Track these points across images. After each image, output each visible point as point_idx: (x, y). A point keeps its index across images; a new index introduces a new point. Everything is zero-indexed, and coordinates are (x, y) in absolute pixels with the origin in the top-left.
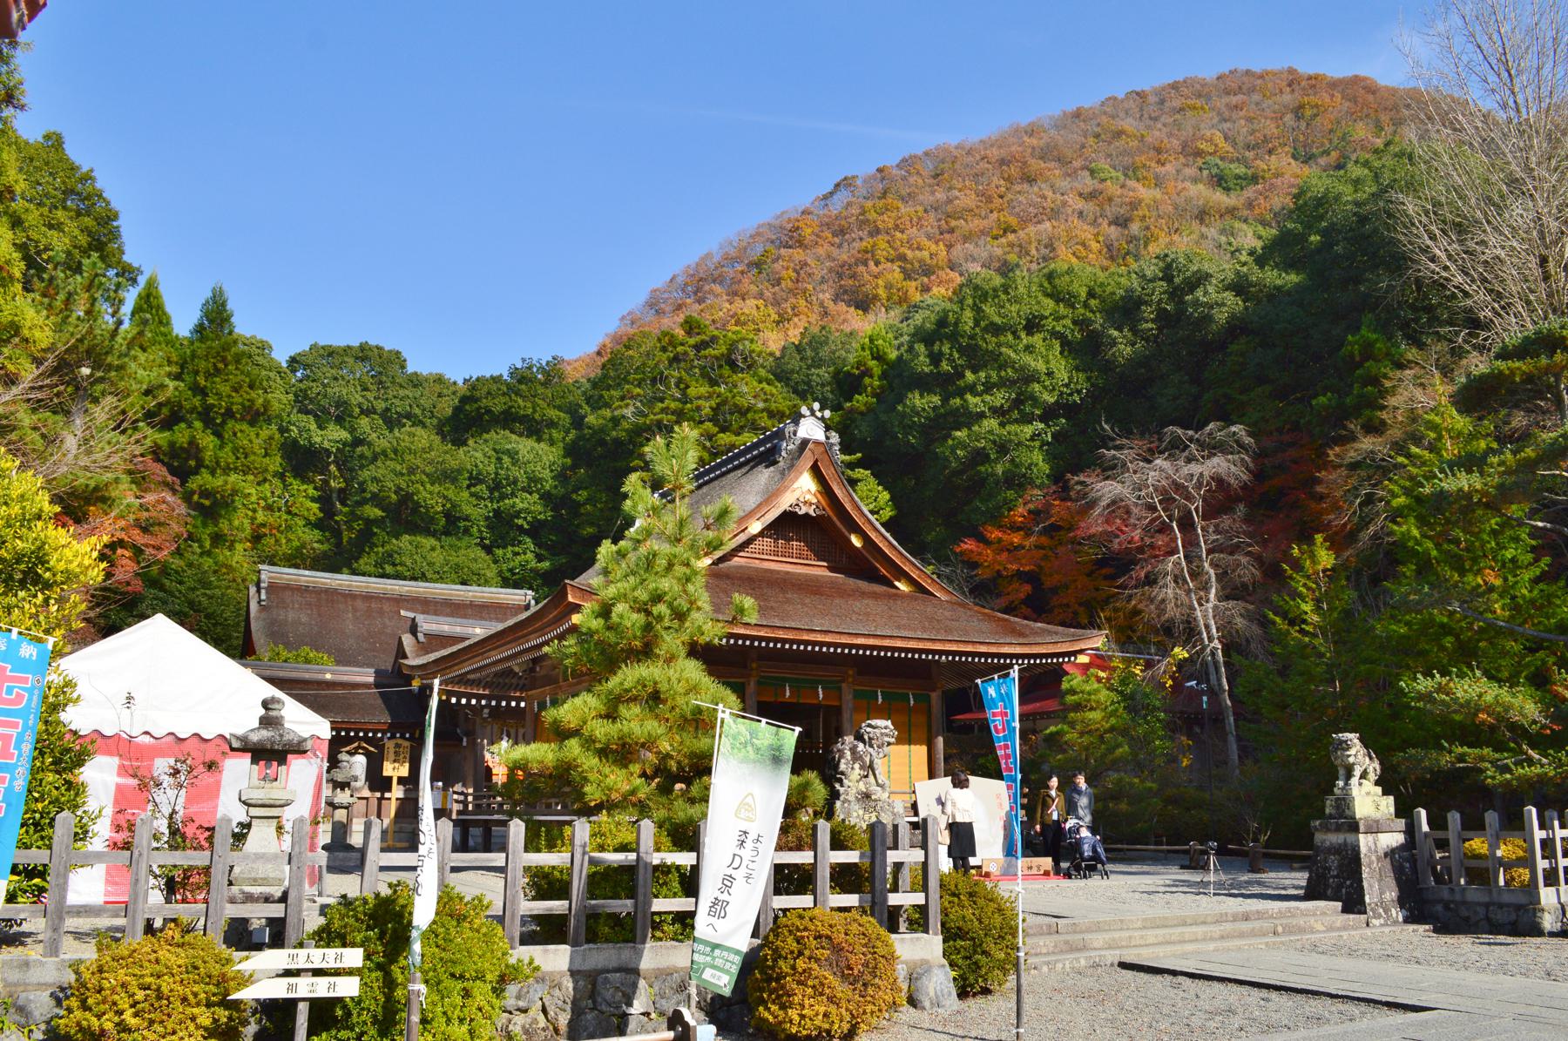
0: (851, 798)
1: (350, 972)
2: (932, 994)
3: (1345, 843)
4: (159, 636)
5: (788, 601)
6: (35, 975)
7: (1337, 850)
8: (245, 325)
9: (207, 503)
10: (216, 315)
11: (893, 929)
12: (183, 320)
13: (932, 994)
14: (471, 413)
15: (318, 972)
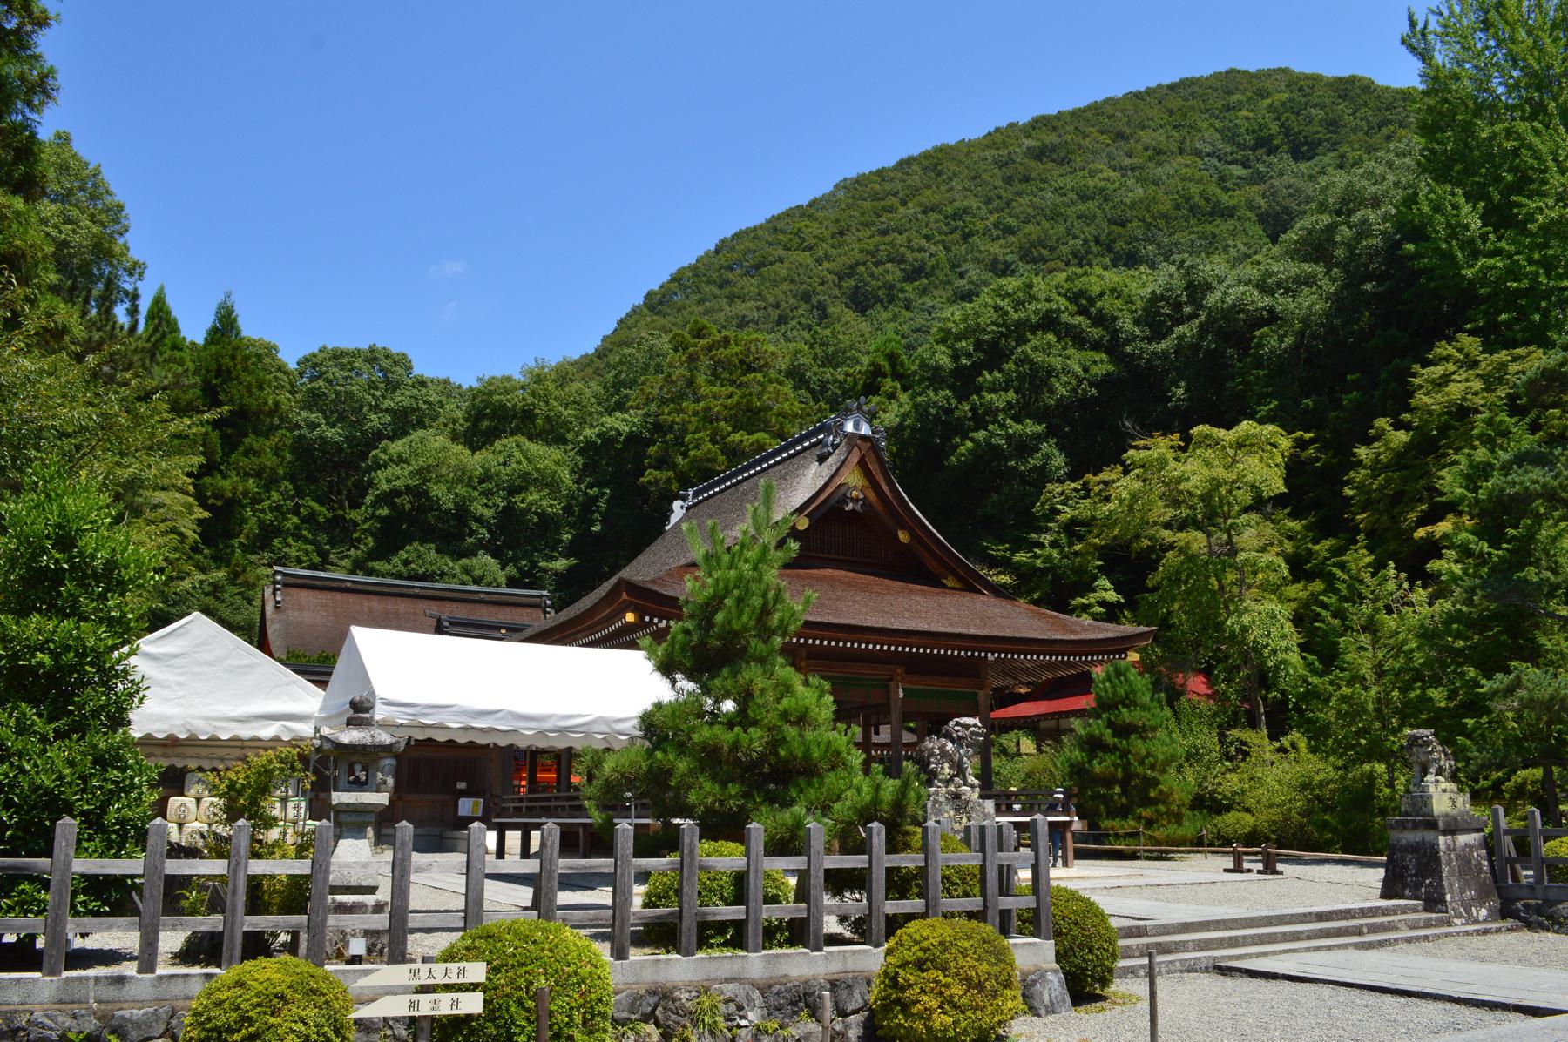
0: (942, 799)
1: (473, 987)
2: (1047, 1001)
3: (1423, 841)
4: (1201, 678)
5: (838, 598)
6: (130, 991)
7: (1415, 848)
8: (251, 328)
9: (219, 503)
10: (225, 324)
11: (1005, 931)
12: (194, 328)
13: (1047, 1001)
14: (490, 416)
15: (448, 988)
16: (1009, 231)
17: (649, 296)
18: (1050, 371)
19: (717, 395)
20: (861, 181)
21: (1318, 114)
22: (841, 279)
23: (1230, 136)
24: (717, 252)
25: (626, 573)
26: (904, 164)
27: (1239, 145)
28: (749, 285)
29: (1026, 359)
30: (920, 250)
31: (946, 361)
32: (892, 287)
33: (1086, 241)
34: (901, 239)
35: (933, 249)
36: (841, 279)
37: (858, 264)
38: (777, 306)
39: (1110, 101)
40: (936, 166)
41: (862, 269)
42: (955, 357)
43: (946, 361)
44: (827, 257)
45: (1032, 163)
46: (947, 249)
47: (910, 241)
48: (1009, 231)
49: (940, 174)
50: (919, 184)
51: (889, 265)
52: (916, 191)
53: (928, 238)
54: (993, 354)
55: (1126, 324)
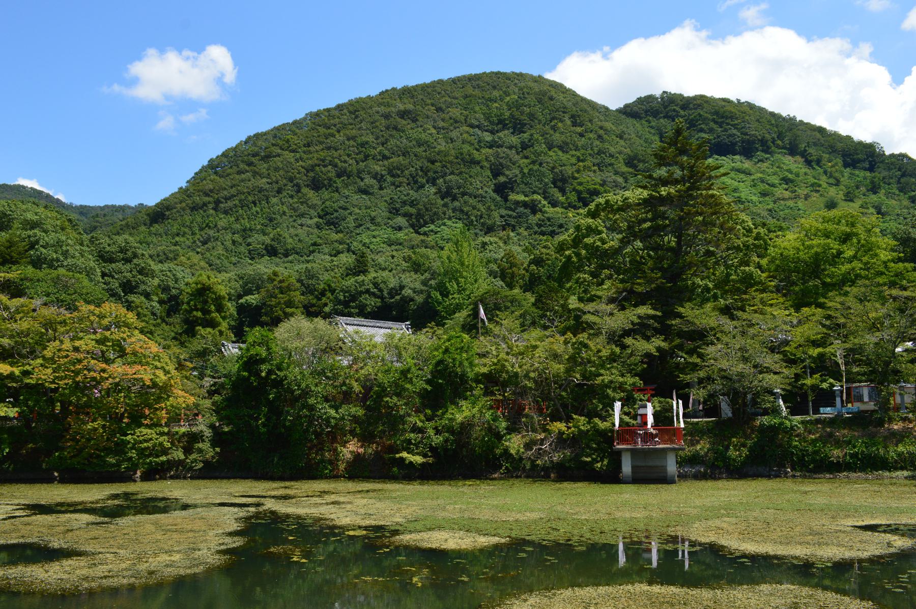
16: (385, 157)
17: (211, 161)
18: (367, 305)
19: (283, 298)
20: (318, 114)
21: (527, 110)
22: (308, 172)
23: (488, 117)
24: (246, 143)
25: (424, 460)
26: (340, 107)
27: (490, 121)
28: (263, 167)
29: (361, 301)
30: (345, 162)
31: (342, 298)
32: (330, 180)
33: (416, 169)
34: (336, 154)
35: (351, 162)
36: (308, 172)
37: (316, 165)
38: (277, 183)
39: (440, 82)
40: (356, 111)
41: (317, 168)
42: (345, 297)
43: (342, 298)
44: (301, 159)
45: (399, 120)
46: (357, 163)
47: (340, 156)
48: (385, 157)
49: (357, 117)
50: (346, 122)
51: (330, 167)
52: (344, 126)
53: (349, 155)
54: (353, 298)
55: (385, 293)
